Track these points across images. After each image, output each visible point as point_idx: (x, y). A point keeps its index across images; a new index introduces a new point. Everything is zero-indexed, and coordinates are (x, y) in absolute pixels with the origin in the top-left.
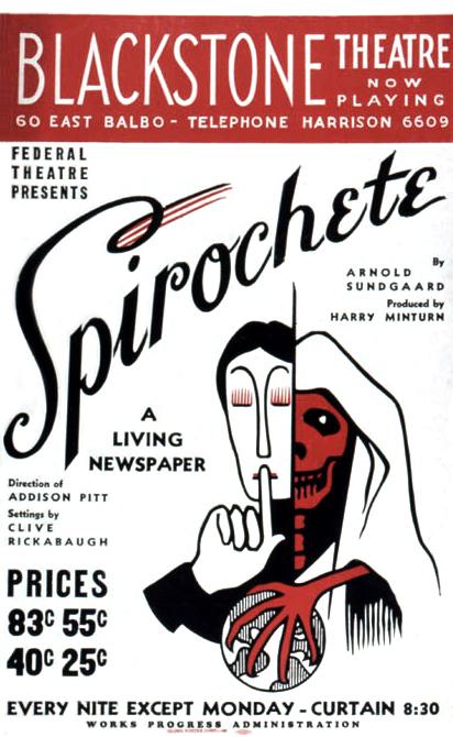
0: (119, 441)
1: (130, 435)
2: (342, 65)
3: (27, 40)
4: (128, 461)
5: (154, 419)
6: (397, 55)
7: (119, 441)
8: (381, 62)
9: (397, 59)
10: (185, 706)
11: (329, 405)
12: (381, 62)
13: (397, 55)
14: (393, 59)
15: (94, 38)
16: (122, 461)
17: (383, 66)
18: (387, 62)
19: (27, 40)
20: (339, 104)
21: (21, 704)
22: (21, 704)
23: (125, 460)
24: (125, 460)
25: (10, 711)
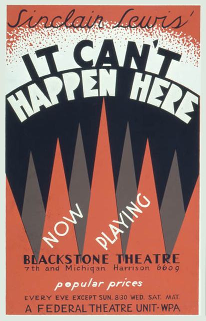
0: (43, 58)
1: (116, 311)
2: (64, 218)
3: (147, 203)
4: (166, 305)
5: (31, 312)
6: (115, 231)
7: (43, 58)
8: (112, 240)
9: (117, 233)
10: (93, 297)
11: (174, 159)
12: (112, 240)
13: (115, 231)
14: (115, 234)
15: (176, 152)
16: (163, 306)
17: (114, 241)
18: (114, 238)
19: (147, 203)
20: (106, 249)
21: (61, 296)
22: (61, 296)
23: (165, 305)
24: (165, 305)
25: (26, 299)
